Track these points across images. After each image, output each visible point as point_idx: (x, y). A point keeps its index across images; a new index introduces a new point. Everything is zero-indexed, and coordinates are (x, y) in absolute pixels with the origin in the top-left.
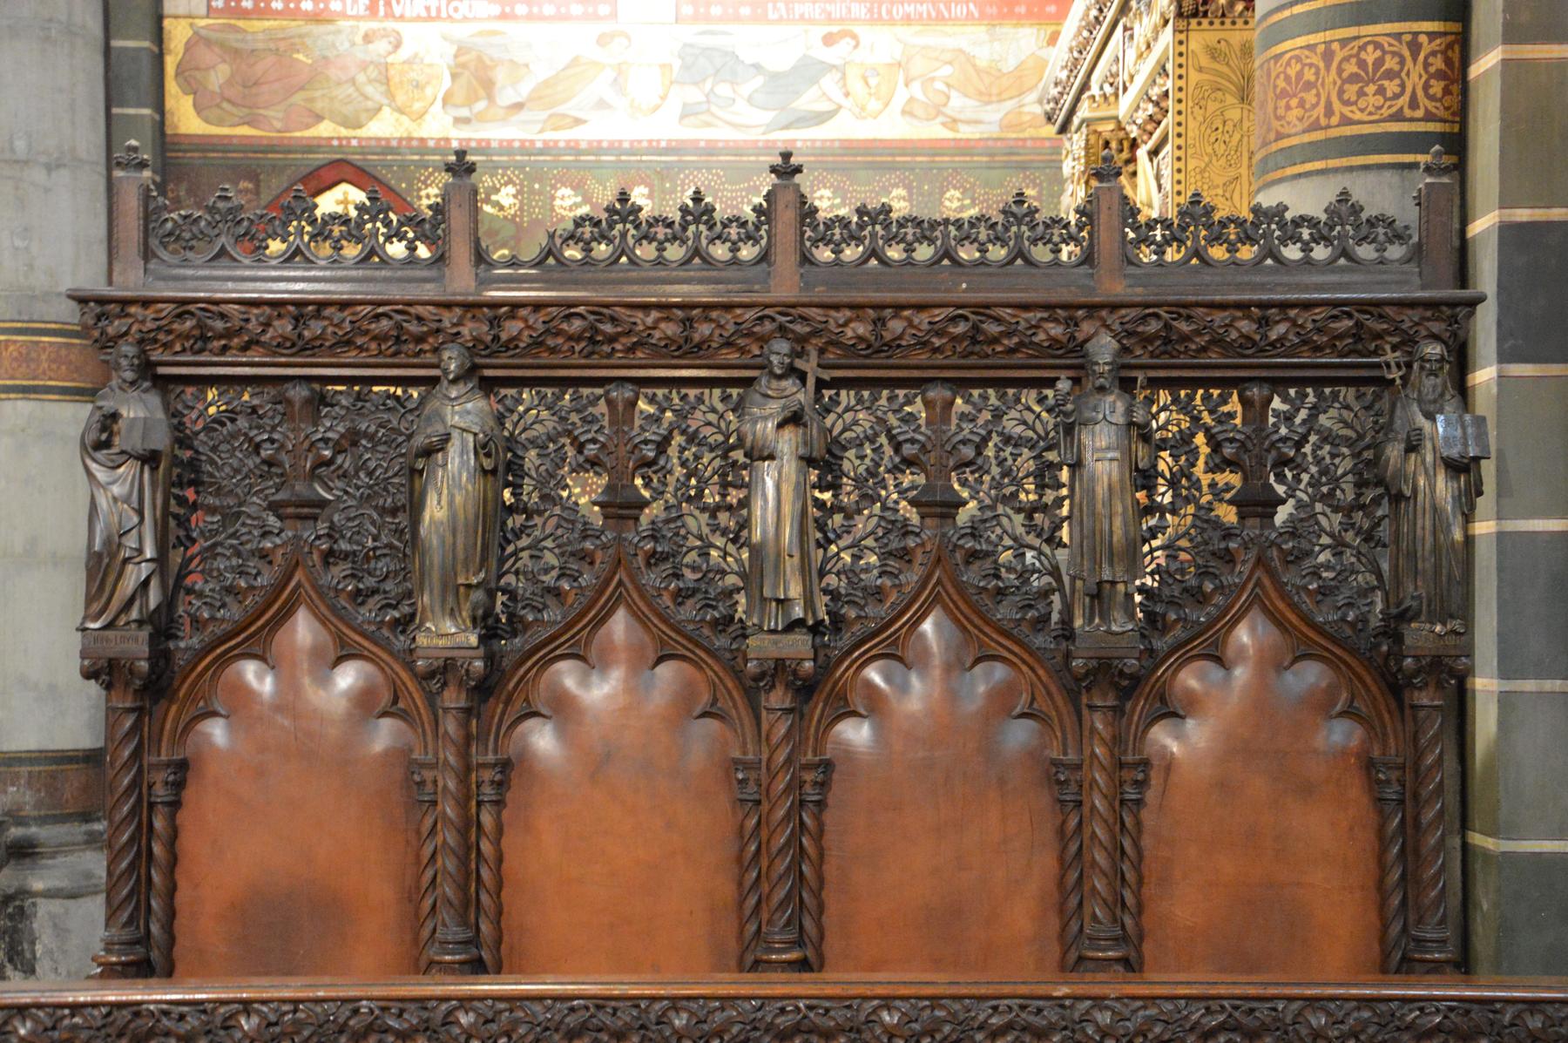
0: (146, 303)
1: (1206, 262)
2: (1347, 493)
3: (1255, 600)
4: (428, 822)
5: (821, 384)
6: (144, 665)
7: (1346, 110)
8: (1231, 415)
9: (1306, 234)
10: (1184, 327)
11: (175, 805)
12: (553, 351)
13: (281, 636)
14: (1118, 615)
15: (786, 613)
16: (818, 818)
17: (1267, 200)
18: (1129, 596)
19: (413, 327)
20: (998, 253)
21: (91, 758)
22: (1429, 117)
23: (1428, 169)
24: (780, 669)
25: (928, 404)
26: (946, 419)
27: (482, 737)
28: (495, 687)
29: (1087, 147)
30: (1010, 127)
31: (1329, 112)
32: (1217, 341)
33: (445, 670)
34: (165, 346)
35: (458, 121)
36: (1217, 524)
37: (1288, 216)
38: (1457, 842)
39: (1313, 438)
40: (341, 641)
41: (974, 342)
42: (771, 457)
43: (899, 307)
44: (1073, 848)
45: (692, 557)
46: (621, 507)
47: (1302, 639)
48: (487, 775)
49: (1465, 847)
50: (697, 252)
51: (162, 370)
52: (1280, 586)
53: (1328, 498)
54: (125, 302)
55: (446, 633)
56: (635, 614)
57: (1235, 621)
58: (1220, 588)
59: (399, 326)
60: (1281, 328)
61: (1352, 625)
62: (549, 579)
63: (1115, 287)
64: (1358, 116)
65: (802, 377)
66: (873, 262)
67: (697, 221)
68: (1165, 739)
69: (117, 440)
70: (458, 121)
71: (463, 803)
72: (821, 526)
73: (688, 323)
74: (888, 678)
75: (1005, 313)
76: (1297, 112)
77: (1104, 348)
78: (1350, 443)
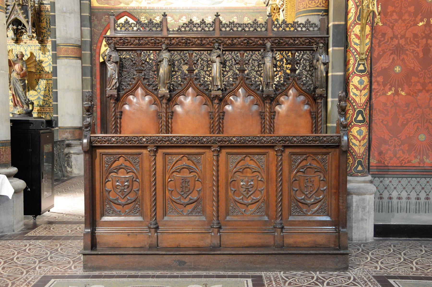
0: (115, 38)
1: (285, 31)
2: (308, 68)
3: (293, 86)
4: (160, 121)
5: (223, 51)
6: (116, 96)
7: (309, 5)
8: (289, 56)
9: (301, 26)
10: (282, 41)
11: (121, 118)
12: (180, 45)
13: (136, 91)
14: (271, 88)
15: (218, 87)
16: (222, 121)
17: (296, 21)
18: (272, 85)
19: (157, 41)
20: (252, 29)
21: (80, 128)
22: (323, 7)
23: (321, 15)
24: (216, 96)
25: (240, 54)
26: (243, 56)
27: (169, 107)
28: (171, 100)
29: (271, 9)
30: (257, 4)
31: (307, 5)
32: (287, 44)
33: (163, 97)
34: (118, 45)
35: (148, 3)
36: (287, 73)
37: (299, 23)
38: (325, 126)
39: (302, 59)
40: (146, 92)
41: (248, 43)
42: (215, 62)
43: (236, 38)
44: (263, 125)
45: (202, 79)
46: (191, 71)
47: (300, 92)
48: (170, 114)
49: (326, 126)
50: (203, 29)
51: (117, 49)
52: (297, 84)
53: (305, 69)
54: (112, 37)
55: (163, 91)
56: (193, 88)
57: (289, 89)
58: (287, 84)
59: (155, 41)
60: (297, 41)
61: (308, 90)
62: (179, 82)
63: (270, 35)
64: (311, 6)
65: (220, 49)
66: (231, 31)
67: (203, 24)
68: (277, 108)
69: (111, 60)
70: (148, 3)
71: (166, 118)
72: (223, 74)
73: (201, 40)
74: (234, 99)
75: (253, 39)
76: (301, 5)
77: (269, 45)
78: (308, 60)
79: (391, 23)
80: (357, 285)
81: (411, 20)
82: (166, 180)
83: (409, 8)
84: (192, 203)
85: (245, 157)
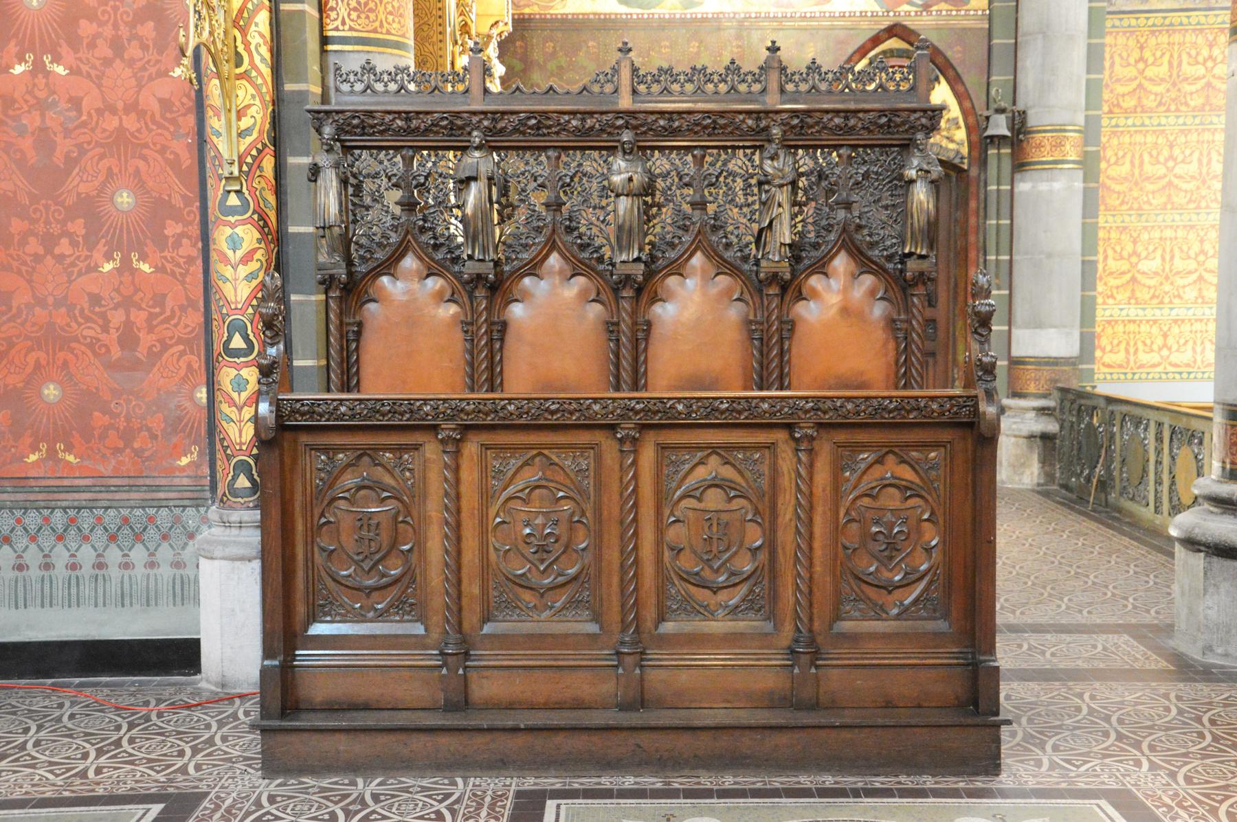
2: (740, 199)
6: (640, 278)
37: (708, 71)
50: (368, 87)
64: (358, 27)
72: (646, 213)
77: (776, 131)
79: (94, 67)
80: (389, 818)
81: (149, 61)
82: (316, 519)
83: (139, 26)
84: (735, 585)
85: (709, 455)
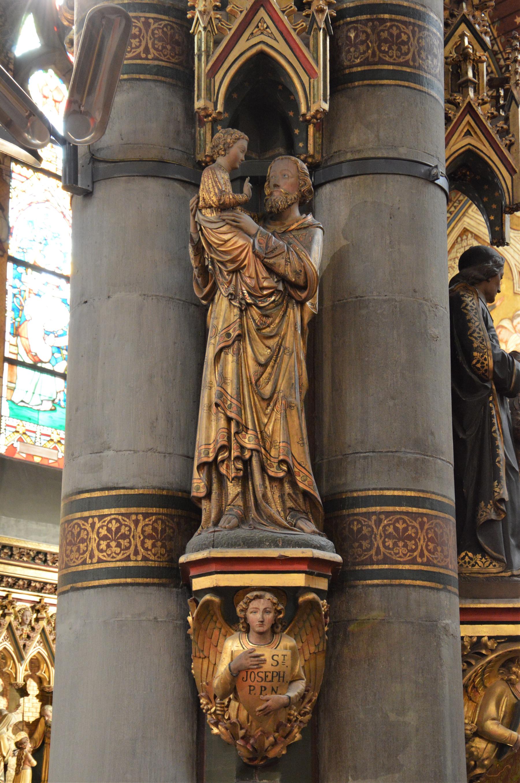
7: (101, 555)
